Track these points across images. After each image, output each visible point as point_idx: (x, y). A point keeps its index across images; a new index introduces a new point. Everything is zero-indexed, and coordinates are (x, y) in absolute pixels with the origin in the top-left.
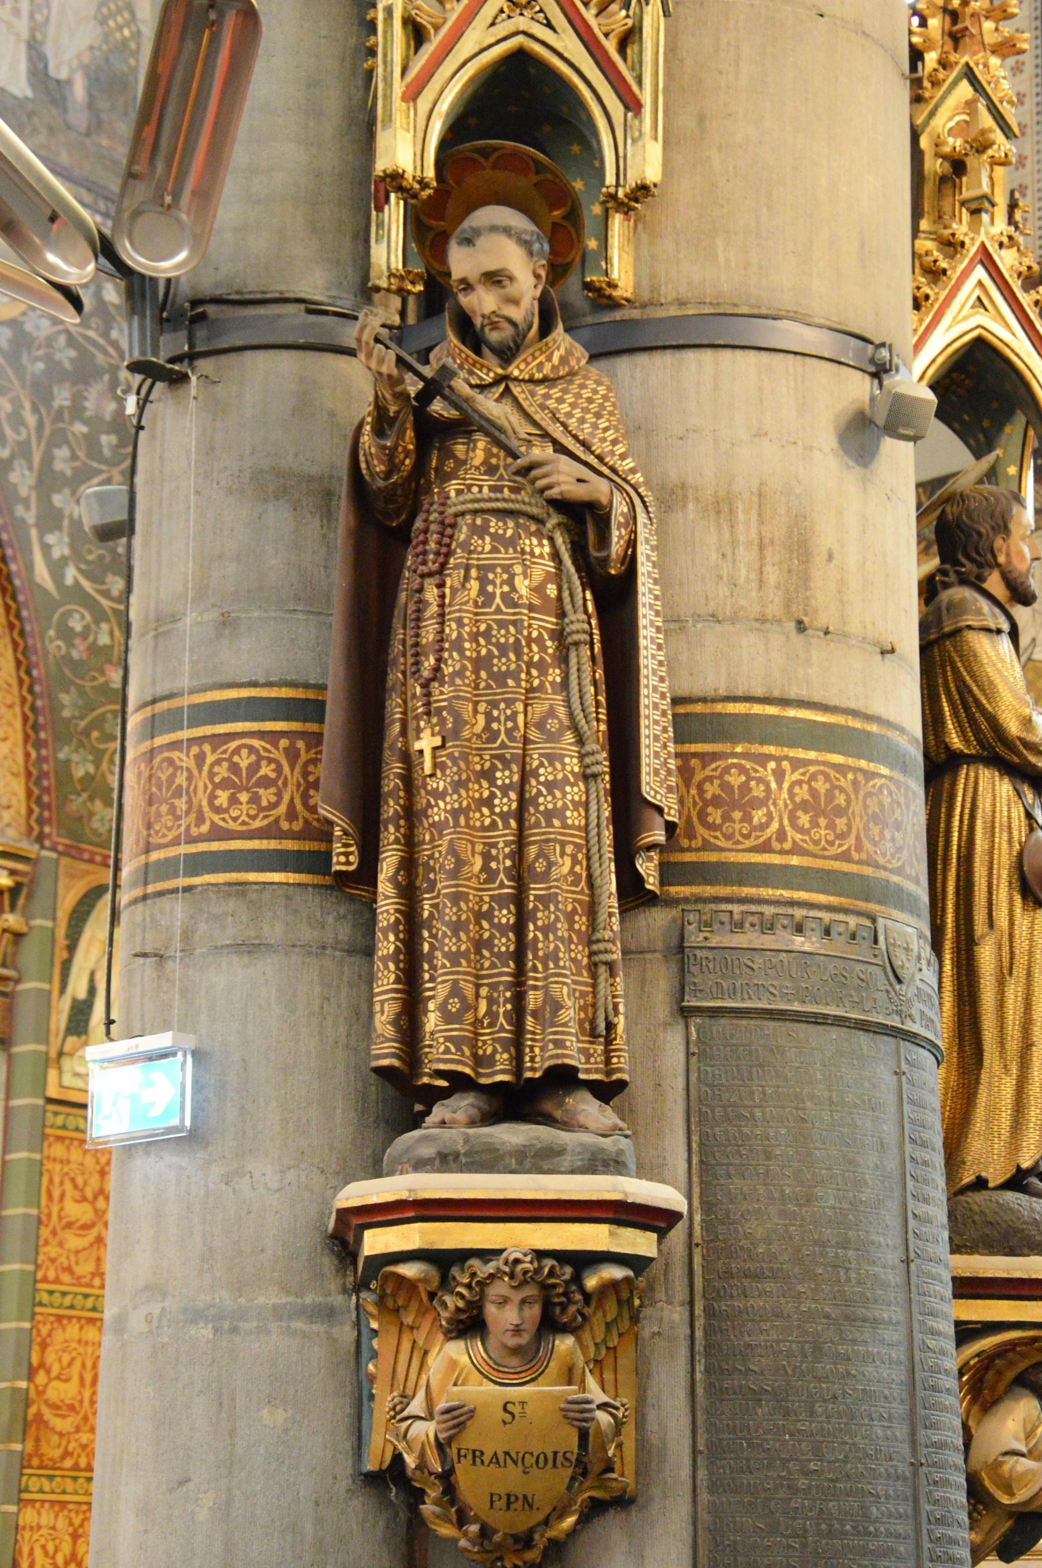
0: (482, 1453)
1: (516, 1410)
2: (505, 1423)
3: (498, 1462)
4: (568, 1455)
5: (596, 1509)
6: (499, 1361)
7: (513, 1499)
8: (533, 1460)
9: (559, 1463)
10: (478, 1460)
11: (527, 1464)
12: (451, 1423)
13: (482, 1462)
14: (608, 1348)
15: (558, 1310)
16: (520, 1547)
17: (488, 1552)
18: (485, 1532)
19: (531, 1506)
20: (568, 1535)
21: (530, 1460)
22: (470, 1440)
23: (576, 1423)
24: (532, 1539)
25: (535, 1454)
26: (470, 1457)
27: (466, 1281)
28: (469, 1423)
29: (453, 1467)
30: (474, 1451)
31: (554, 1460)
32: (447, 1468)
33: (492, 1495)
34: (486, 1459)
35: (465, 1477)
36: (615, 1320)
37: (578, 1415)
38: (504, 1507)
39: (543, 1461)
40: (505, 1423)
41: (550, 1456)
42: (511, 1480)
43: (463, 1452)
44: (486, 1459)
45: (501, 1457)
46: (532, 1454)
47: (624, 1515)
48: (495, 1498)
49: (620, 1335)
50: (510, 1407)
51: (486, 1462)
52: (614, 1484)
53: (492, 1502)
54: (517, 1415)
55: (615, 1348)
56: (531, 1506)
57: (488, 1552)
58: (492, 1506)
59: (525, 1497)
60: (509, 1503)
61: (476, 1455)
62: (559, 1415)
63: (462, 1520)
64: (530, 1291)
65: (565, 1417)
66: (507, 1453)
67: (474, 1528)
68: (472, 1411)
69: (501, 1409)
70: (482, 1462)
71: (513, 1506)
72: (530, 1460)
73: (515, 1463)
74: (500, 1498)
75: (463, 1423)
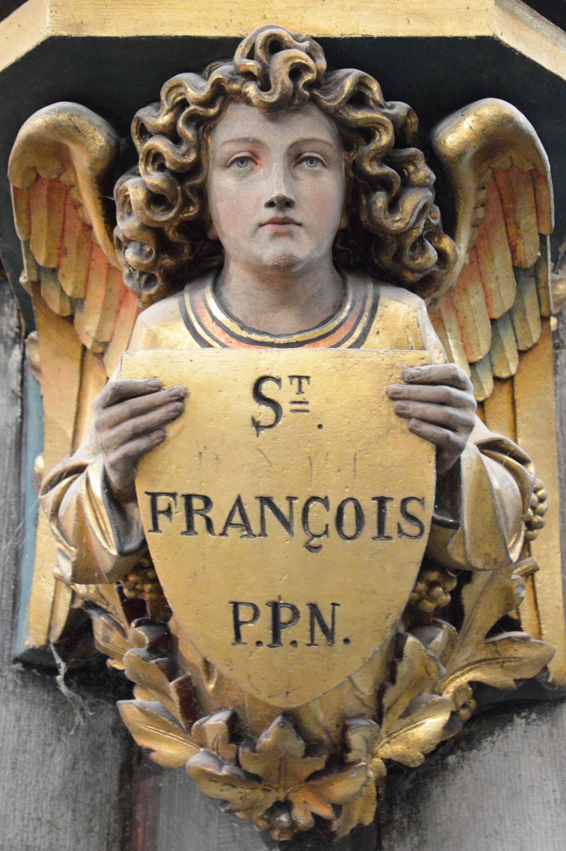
0: (207, 502)
1: (284, 395)
2: (257, 425)
3: (246, 524)
4: (412, 507)
5: (489, 712)
6: (250, 322)
7: (285, 615)
8: (330, 517)
9: (390, 528)
10: (199, 522)
11: (315, 527)
12: (128, 426)
13: (209, 524)
14: (497, 380)
15: (380, 200)
16: (319, 763)
17: (253, 779)
18: (237, 731)
19: (329, 634)
20: (429, 756)
21: (321, 517)
22: (172, 471)
23: (426, 428)
24: (345, 747)
25: (334, 505)
26: (179, 513)
27: (164, 119)
28: (172, 430)
29: (144, 543)
30: (188, 498)
31: (375, 516)
32: (132, 545)
33: (236, 605)
34: (218, 515)
35: (173, 557)
36: (510, 313)
37: (432, 410)
38: (267, 638)
39: (349, 518)
40: (257, 425)
41: (370, 509)
42: (273, 566)
43: (162, 503)
44: (218, 515)
45: (252, 509)
46: (325, 501)
47: (545, 728)
48: (245, 614)
49: (522, 353)
50: (267, 389)
51: (218, 527)
52: (522, 651)
53: (237, 624)
54: (286, 407)
55: (511, 379)
56: (329, 634)
57: (253, 779)
58: (238, 636)
59: (313, 607)
60: (277, 626)
61: (194, 507)
62: (387, 408)
63: (192, 706)
64: (311, 128)
65: (402, 415)
66: (266, 501)
67: (215, 722)
68: (181, 398)
69: (249, 392)
70: (209, 524)
71: (286, 634)
72: (321, 517)
73: (287, 524)
74: (256, 614)
75: (161, 425)
